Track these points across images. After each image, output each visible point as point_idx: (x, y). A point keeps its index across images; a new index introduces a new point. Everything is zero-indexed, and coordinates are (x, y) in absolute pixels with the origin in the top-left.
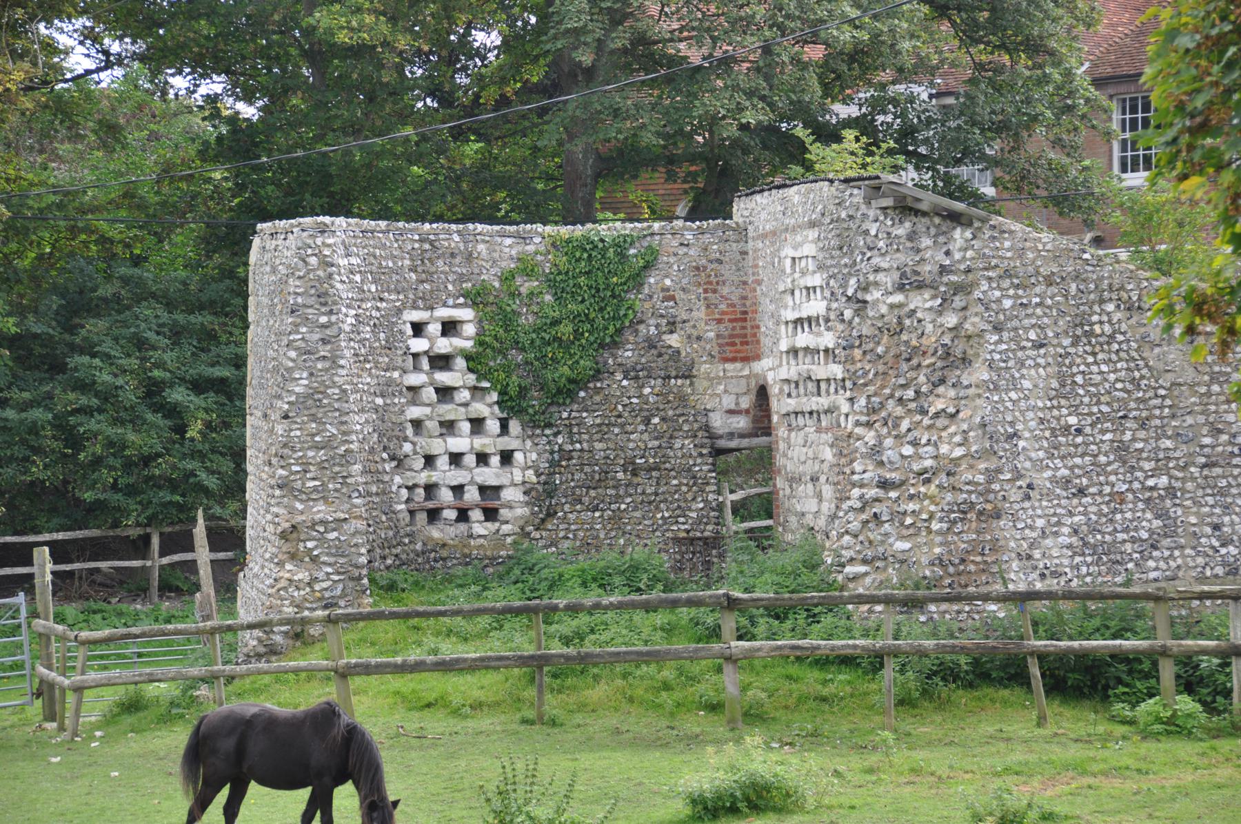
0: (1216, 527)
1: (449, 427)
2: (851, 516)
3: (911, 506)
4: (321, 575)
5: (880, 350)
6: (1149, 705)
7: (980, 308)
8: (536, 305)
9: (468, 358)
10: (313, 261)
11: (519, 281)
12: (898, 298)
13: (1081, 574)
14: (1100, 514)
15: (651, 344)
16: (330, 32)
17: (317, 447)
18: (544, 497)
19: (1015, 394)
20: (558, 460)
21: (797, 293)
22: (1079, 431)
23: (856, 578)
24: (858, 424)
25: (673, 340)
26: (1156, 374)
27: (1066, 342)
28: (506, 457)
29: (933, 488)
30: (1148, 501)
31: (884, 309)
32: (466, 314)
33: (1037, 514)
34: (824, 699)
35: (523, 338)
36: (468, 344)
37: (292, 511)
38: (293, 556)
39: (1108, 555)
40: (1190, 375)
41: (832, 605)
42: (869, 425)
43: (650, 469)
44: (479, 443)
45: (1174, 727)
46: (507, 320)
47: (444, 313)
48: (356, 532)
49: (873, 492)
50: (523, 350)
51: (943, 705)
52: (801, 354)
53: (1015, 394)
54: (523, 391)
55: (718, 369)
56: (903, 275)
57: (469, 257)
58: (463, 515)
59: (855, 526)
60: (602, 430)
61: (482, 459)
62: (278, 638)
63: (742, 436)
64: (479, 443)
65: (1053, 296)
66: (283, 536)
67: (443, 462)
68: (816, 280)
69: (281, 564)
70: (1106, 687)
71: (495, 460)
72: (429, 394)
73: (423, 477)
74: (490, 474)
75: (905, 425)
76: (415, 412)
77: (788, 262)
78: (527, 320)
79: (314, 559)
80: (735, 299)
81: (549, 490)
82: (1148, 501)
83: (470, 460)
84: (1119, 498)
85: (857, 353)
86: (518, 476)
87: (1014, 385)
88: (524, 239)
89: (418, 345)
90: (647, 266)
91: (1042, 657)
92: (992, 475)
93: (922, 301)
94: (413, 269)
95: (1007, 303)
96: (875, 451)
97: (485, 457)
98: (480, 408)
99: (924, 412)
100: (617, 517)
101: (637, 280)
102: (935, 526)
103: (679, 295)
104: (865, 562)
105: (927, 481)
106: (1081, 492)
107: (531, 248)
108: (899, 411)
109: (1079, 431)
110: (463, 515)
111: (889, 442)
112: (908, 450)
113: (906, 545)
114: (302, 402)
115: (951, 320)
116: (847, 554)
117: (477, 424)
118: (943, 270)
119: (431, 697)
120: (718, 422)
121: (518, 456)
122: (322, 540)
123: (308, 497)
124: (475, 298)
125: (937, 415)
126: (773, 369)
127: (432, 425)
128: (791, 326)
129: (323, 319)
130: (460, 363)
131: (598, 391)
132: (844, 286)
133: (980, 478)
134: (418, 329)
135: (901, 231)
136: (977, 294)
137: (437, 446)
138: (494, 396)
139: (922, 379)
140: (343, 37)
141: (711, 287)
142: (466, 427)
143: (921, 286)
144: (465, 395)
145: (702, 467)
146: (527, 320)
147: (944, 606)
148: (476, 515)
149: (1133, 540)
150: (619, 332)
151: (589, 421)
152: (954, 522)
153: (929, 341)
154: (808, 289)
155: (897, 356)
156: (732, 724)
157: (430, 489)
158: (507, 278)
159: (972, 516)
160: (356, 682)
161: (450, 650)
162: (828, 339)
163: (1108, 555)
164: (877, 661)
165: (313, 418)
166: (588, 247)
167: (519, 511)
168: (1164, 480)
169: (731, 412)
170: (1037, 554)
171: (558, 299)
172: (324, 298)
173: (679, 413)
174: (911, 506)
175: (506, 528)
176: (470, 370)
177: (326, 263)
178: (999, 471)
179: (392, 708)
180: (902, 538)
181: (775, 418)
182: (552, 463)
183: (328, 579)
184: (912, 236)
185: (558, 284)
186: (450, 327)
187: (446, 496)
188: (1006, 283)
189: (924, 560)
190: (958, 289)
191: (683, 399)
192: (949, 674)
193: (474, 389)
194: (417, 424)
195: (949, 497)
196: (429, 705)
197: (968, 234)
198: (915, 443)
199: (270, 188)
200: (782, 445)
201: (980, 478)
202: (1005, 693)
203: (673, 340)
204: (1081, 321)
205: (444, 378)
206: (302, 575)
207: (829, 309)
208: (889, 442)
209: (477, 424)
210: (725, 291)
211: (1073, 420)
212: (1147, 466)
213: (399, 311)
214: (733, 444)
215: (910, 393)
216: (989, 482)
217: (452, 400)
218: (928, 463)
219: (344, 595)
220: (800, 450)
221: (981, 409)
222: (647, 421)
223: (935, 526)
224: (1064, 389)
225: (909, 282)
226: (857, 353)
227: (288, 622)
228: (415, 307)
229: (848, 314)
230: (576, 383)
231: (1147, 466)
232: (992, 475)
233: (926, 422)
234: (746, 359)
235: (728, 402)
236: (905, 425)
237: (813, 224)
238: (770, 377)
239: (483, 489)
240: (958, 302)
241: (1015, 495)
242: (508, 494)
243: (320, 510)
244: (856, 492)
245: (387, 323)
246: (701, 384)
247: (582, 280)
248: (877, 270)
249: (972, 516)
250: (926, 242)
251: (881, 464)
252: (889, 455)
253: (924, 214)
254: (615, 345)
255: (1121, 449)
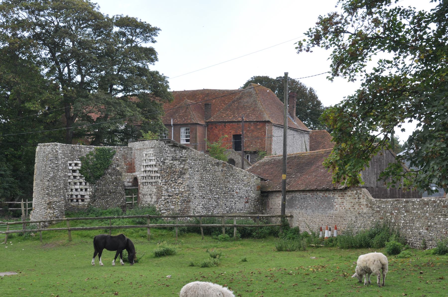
0: (225, 204)
1: (75, 184)
2: (162, 201)
3: (174, 200)
4: (55, 212)
5: (167, 171)
6: (220, 236)
7: (188, 164)
8: (92, 160)
9: (80, 170)
10: (54, 151)
11: (89, 156)
12: (172, 162)
13: (204, 213)
14: (207, 202)
15: (114, 169)
16: (29, 108)
17: (54, 187)
18: (93, 197)
19: (193, 180)
20: (96, 190)
21: (147, 160)
22: (204, 187)
23: (164, 213)
24: (163, 184)
25: (118, 168)
26: (217, 177)
27: (202, 171)
28: (86, 190)
29: (178, 197)
30: (215, 200)
31: (169, 164)
32: (79, 162)
33: (196, 202)
34: (163, 235)
35: (90, 167)
36: (80, 168)
37: (49, 199)
38: (50, 208)
39: (208, 209)
40: (222, 178)
41: (160, 218)
42: (165, 185)
43: (113, 192)
44: (81, 187)
45: (225, 240)
46: (87, 163)
47: (75, 162)
48: (63, 203)
49: (167, 197)
50: (90, 169)
51: (184, 236)
52: (147, 172)
53: (193, 180)
54: (90, 177)
55: (126, 174)
56: (173, 158)
57: (80, 151)
58: (77, 201)
59: (163, 203)
60: (105, 185)
61: (81, 190)
62: (47, 224)
63: (130, 187)
64: (81, 187)
65: (200, 163)
66: (48, 204)
67: (74, 190)
68: (153, 158)
69: (47, 209)
70: (210, 233)
71: (84, 190)
72: (72, 177)
73: (70, 193)
74: (83, 193)
75: (173, 185)
76: (69, 181)
77: (144, 155)
78: (91, 164)
79: (54, 209)
80: (130, 161)
81: (95, 196)
82: (215, 200)
83: (79, 190)
84: (210, 199)
85: (163, 172)
86: (88, 194)
87: (193, 178)
88: (91, 148)
89: (70, 168)
90: (114, 154)
91: (203, 227)
92: (189, 194)
93: (176, 163)
94: (70, 153)
95: (193, 163)
96: (167, 190)
97: (82, 190)
98: (81, 180)
99: (176, 183)
100: (107, 201)
101: (112, 157)
102: (179, 203)
103: (119, 160)
104: (165, 210)
105: (177, 195)
106: (204, 198)
107: (92, 150)
108: (171, 182)
109: (204, 187)
110: (77, 201)
111: (169, 188)
112: (173, 190)
113: (174, 207)
114: (52, 178)
115: (182, 166)
116: (162, 208)
117: (81, 183)
118: (181, 157)
119: (86, 234)
120: (126, 184)
121: (88, 190)
122: (56, 205)
123: (53, 196)
124: (81, 159)
125: (179, 183)
126: (139, 174)
127: (72, 183)
128: (144, 167)
129: (56, 162)
130: (78, 171)
131: (104, 177)
132: (161, 159)
133: (187, 195)
134: (70, 165)
135: (173, 150)
136: (187, 162)
137: (73, 187)
138: (84, 178)
139: (176, 177)
140: (32, 109)
141: (125, 159)
142: (79, 184)
143: (176, 160)
144: (79, 178)
145: (123, 192)
146: (91, 164)
147: (181, 218)
148: (80, 201)
149: (212, 207)
150: (108, 166)
151: (102, 183)
152: (182, 203)
153: (177, 170)
154: (150, 160)
155: (171, 172)
156: (148, 240)
157: (72, 195)
158: (87, 156)
159: (185, 202)
160: (72, 232)
161: (86, 226)
162: (156, 169)
163: (208, 209)
164: (171, 229)
165: (54, 181)
166: (103, 150)
167: (89, 200)
168: (217, 196)
169: (128, 182)
170: (196, 209)
171: (97, 160)
172: (56, 158)
173: (119, 182)
174: (174, 200)
175: (86, 203)
176: (80, 173)
177: (57, 152)
178: (190, 194)
179: (78, 237)
180: (173, 206)
181: (139, 183)
182: (95, 191)
183: (57, 212)
184: (175, 151)
185: (97, 157)
186: (76, 165)
187: (74, 197)
188: (192, 160)
189: (177, 210)
190: (184, 160)
191: (119, 179)
192: (184, 230)
193: (80, 176)
194: (69, 183)
195: (182, 198)
196: (85, 236)
197: (186, 151)
198: (175, 188)
199: (12, 137)
200: (141, 188)
201: (187, 195)
202: (194, 234)
203: (118, 168)
204: (205, 167)
205: (74, 174)
206: (52, 212)
207: (156, 163)
208: (169, 188)
209: (81, 183)
210: (128, 159)
211: (203, 185)
212: (215, 193)
213: (67, 161)
214: (128, 188)
215: (174, 179)
216: (189, 196)
217: (76, 178)
218: (178, 192)
219: (60, 215)
220: (144, 189)
221: (187, 183)
222: (113, 183)
223: (179, 203)
224: (202, 179)
225: (174, 159)
226: (163, 172)
227: (49, 221)
228: (70, 161)
229: (161, 164)
230: (101, 176)
231: (215, 193)
232: (189, 194)
233: (177, 184)
234: (131, 172)
235: (128, 180)
236: (173, 185)
237: (152, 148)
238: (138, 176)
239: (81, 196)
240: (183, 163)
241: (193, 198)
242: (86, 197)
243: (55, 199)
244: (163, 197)
245: (65, 163)
246: (123, 177)
247: (102, 157)
248: (168, 157)
249: (185, 202)
250: (178, 152)
251: (168, 192)
252: (169, 190)
253: (177, 147)
254: (107, 169)
255: (211, 190)
